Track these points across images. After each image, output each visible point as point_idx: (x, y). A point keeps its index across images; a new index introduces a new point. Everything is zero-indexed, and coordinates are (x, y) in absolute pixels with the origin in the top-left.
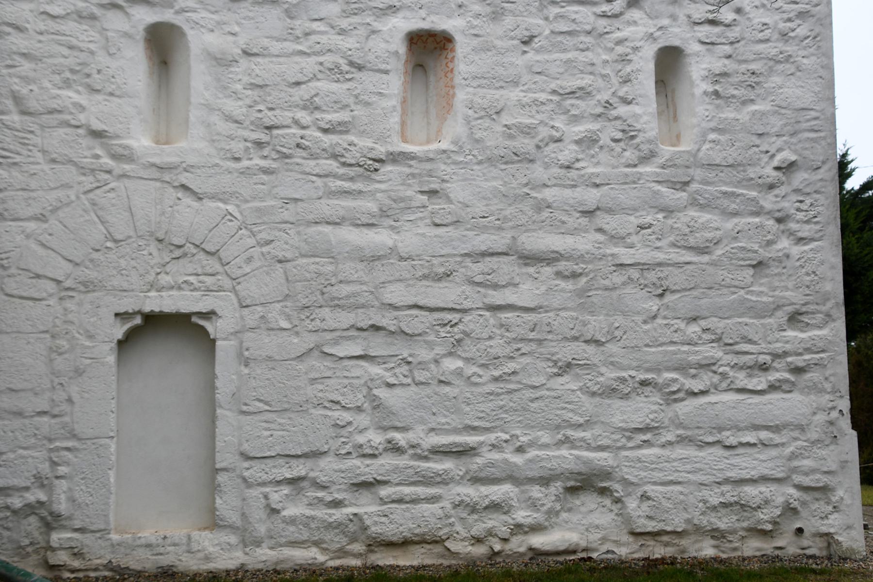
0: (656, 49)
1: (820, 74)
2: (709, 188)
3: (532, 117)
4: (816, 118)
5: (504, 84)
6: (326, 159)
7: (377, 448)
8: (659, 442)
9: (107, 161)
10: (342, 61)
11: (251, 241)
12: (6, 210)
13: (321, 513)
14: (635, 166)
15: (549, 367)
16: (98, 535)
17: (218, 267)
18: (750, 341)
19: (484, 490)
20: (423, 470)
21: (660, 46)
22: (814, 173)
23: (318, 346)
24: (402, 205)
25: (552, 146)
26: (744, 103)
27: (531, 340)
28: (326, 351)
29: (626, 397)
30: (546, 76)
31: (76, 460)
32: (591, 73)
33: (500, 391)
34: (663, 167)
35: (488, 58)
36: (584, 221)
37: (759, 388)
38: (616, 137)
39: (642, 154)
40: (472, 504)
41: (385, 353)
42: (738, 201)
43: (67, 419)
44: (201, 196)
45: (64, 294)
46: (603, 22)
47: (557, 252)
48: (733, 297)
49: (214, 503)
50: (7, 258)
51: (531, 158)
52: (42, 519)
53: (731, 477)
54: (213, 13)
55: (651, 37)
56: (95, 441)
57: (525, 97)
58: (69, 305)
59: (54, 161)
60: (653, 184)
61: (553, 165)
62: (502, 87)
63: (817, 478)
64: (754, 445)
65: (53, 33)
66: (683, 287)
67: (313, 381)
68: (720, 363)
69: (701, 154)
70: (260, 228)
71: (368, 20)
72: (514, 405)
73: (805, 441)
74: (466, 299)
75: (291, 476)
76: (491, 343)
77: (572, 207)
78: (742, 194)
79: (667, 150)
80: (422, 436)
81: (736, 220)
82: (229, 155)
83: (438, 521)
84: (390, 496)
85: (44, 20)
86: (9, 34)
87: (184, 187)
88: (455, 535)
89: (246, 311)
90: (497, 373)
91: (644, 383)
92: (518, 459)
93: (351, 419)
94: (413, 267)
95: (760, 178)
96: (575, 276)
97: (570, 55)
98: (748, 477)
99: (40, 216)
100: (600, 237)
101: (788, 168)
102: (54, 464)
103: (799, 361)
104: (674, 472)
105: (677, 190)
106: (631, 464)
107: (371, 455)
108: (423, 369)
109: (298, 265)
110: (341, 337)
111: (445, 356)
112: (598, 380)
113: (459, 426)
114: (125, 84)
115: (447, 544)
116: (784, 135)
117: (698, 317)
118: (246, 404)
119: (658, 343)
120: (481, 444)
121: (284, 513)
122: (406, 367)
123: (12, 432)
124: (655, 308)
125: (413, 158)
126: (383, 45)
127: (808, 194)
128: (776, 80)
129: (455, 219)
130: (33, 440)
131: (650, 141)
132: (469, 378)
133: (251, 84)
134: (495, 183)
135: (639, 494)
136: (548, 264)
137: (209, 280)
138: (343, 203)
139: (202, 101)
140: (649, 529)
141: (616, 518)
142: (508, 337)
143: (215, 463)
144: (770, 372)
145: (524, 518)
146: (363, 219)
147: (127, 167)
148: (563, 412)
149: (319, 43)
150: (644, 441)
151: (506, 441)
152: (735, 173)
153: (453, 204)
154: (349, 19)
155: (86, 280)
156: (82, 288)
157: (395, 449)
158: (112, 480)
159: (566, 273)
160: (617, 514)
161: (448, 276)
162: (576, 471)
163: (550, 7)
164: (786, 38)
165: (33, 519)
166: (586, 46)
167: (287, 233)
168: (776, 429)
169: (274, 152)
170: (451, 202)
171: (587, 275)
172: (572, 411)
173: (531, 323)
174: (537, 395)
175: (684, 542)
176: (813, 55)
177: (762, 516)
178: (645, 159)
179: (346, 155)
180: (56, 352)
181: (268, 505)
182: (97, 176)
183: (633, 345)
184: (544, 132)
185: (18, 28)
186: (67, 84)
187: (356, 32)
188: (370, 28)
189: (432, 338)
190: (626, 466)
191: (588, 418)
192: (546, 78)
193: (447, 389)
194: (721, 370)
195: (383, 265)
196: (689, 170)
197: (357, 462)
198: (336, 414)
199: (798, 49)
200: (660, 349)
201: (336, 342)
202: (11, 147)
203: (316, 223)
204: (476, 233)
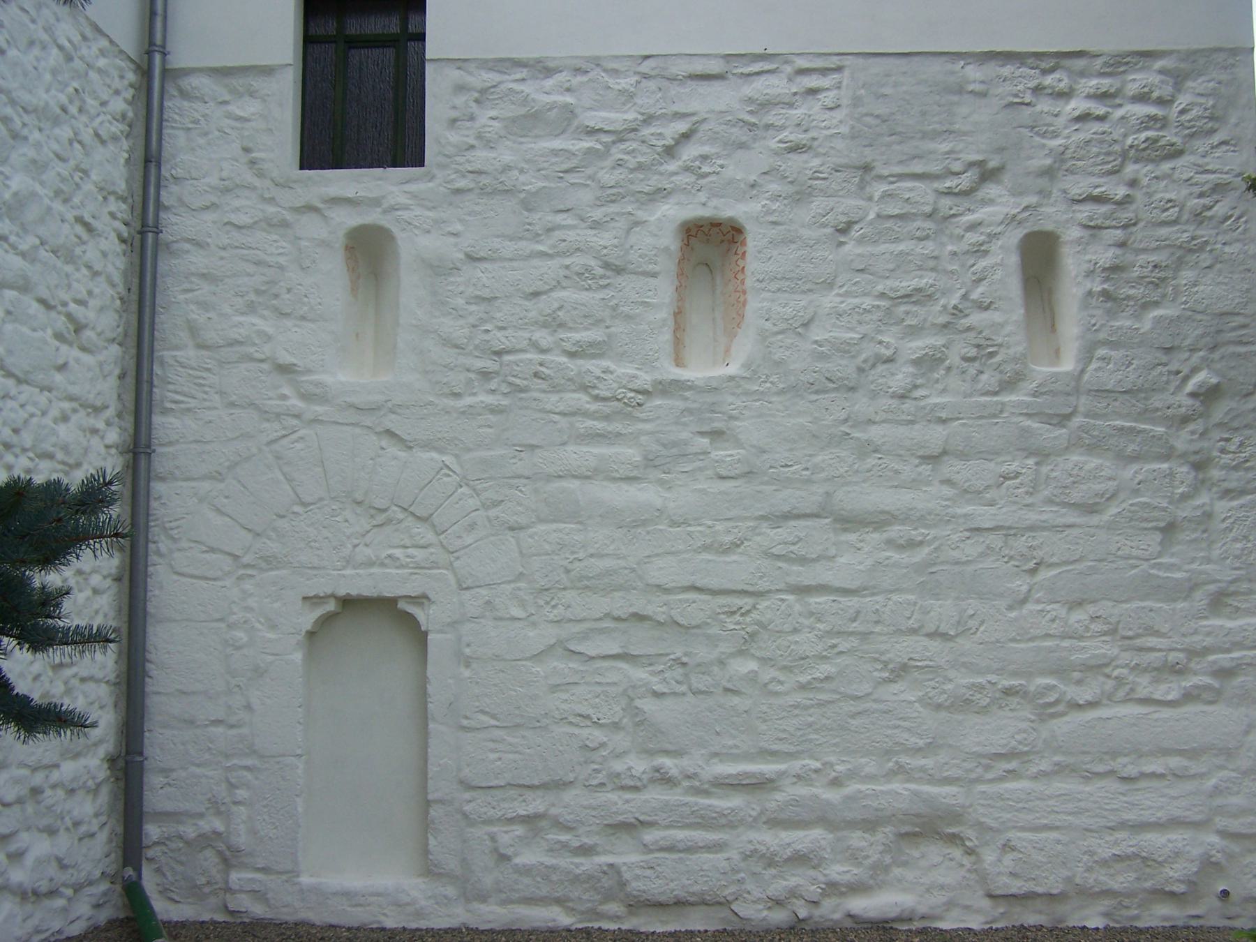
0: (1021, 235)
1: (1248, 267)
2: (1098, 422)
3: (852, 329)
4: (1244, 326)
5: (814, 287)
6: (574, 391)
7: (639, 779)
8: (1029, 772)
9: (296, 403)
10: (593, 263)
11: (473, 502)
12: (177, 467)
13: (565, 862)
14: (996, 393)
15: (876, 670)
16: (284, 877)
17: (430, 537)
18: (1157, 634)
19: (786, 836)
20: (702, 809)
21: (1025, 231)
22: (1243, 401)
23: (561, 642)
24: (674, 451)
25: (881, 368)
26: (1146, 306)
27: (852, 634)
28: (573, 649)
29: (984, 710)
30: (871, 274)
31: (257, 782)
32: (933, 270)
33: (809, 702)
34: (1035, 394)
35: (791, 253)
36: (926, 469)
37: (1170, 697)
38: (969, 355)
39: (1006, 377)
40: (768, 855)
41: (652, 651)
42: (1138, 439)
43: (245, 731)
44: (411, 444)
45: (241, 572)
46: (946, 202)
47: (888, 513)
48: (1133, 572)
49: (427, 845)
50: (177, 527)
51: (851, 385)
52: (220, 853)
53: (1129, 820)
54: (429, 209)
55: (1012, 220)
56: (278, 759)
57: (842, 302)
58: (248, 587)
59: (233, 405)
60: (1021, 419)
61: (882, 393)
62: (810, 290)
63: (1249, 821)
64: (1162, 776)
65: (237, 247)
66: (1064, 559)
67: (555, 688)
68: (1114, 664)
69: (1086, 377)
70: (484, 485)
71: (629, 209)
72: (828, 722)
73: (1233, 770)
74: (761, 578)
75: (525, 813)
76: (796, 638)
77: (909, 450)
78: (1144, 431)
79: (1043, 370)
80: (700, 763)
81: (1135, 467)
82: (446, 390)
83: (721, 877)
84: (657, 841)
85: (228, 232)
86: (188, 252)
87: (390, 433)
88: (745, 895)
89: (467, 595)
90: (804, 679)
91: (1008, 692)
92: (832, 795)
93: (605, 739)
94: (689, 534)
95: (1169, 408)
96: (912, 545)
97: (901, 247)
98: (1153, 819)
99: (214, 474)
100: (947, 491)
101: (1209, 395)
102: (232, 786)
103: (1223, 659)
104: (1049, 812)
105: (1054, 425)
106: (989, 802)
107: (631, 787)
108: (703, 673)
109: (536, 533)
110: (592, 630)
111: (733, 655)
112: (945, 687)
113: (752, 751)
114: (320, 304)
115: (734, 907)
116: (1201, 350)
117: (1084, 600)
118: (467, 718)
119: (1029, 636)
120: (782, 774)
121: (517, 860)
122: (681, 670)
123: (183, 744)
124: (1024, 588)
125: (690, 388)
126: (649, 240)
127: (1237, 429)
128: (1187, 275)
129: (747, 470)
130: (207, 756)
131: (1015, 360)
132: (765, 685)
133: (477, 297)
134: (801, 420)
135: (999, 844)
136: (875, 530)
137: (419, 554)
138: (596, 451)
139: (414, 322)
140: (1014, 891)
141: (968, 875)
142: (820, 630)
143: (427, 793)
145: (839, 874)
146: (621, 471)
147: (319, 409)
148: (896, 731)
149: (564, 241)
150: (1009, 772)
151: (816, 771)
152: (1134, 402)
153: (744, 448)
154: (604, 209)
155: (268, 554)
156: (263, 565)
157: (663, 779)
158: (300, 809)
159: (902, 541)
160: (969, 871)
161: (738, 546)
162: (913, 812)
163: (875, 184)
164: (1199, 218)
165: (209, 853)
166: (925, 234)
167: (521, 491)
168: (1193, 754)
169: (504, 385)
170: (741, 446)
171: (929, 543)
172: (909, 730)
173: (851, 611)
174: (860, 709)
175: (1061, 909)
176: (1238, 240)
177: (1171, 874)
178: (1009, 385)
179: (600, 386)
180: (233, 645)
181: (496, 850)
182: (283, 422)
183: (993, 639)
184: (869, 350)
185: (199, 244)
186: (251, 308)
187: (613, 224)
188: (633, 218)
189: (715, 630)
190: (983, 805)
191: (928, 741)
192: (871, 277)
193: (736, 700)
194: (1116, 673)
195: (648, 533)
196: (1071, 398)
197: (613, 796)
198: (585, 733)
199: (1217, 234)
200: (1031, 644)
201: (585, 636)
202: (185, 389)
203: (560, 477)
204: (774, 488)
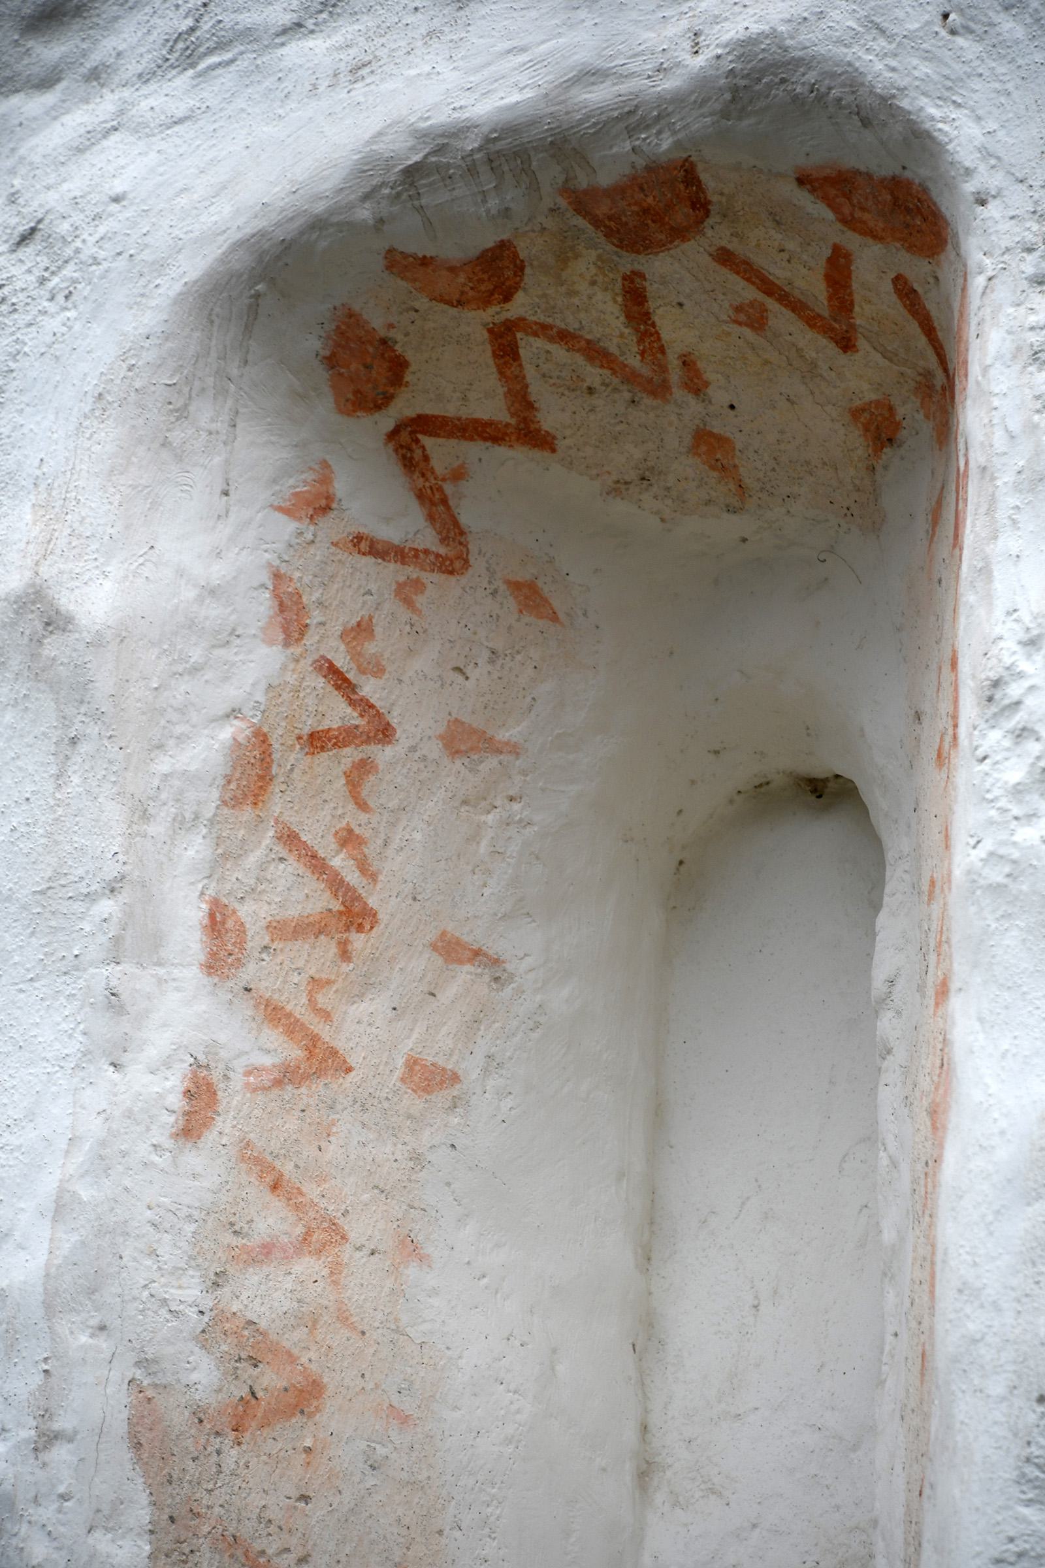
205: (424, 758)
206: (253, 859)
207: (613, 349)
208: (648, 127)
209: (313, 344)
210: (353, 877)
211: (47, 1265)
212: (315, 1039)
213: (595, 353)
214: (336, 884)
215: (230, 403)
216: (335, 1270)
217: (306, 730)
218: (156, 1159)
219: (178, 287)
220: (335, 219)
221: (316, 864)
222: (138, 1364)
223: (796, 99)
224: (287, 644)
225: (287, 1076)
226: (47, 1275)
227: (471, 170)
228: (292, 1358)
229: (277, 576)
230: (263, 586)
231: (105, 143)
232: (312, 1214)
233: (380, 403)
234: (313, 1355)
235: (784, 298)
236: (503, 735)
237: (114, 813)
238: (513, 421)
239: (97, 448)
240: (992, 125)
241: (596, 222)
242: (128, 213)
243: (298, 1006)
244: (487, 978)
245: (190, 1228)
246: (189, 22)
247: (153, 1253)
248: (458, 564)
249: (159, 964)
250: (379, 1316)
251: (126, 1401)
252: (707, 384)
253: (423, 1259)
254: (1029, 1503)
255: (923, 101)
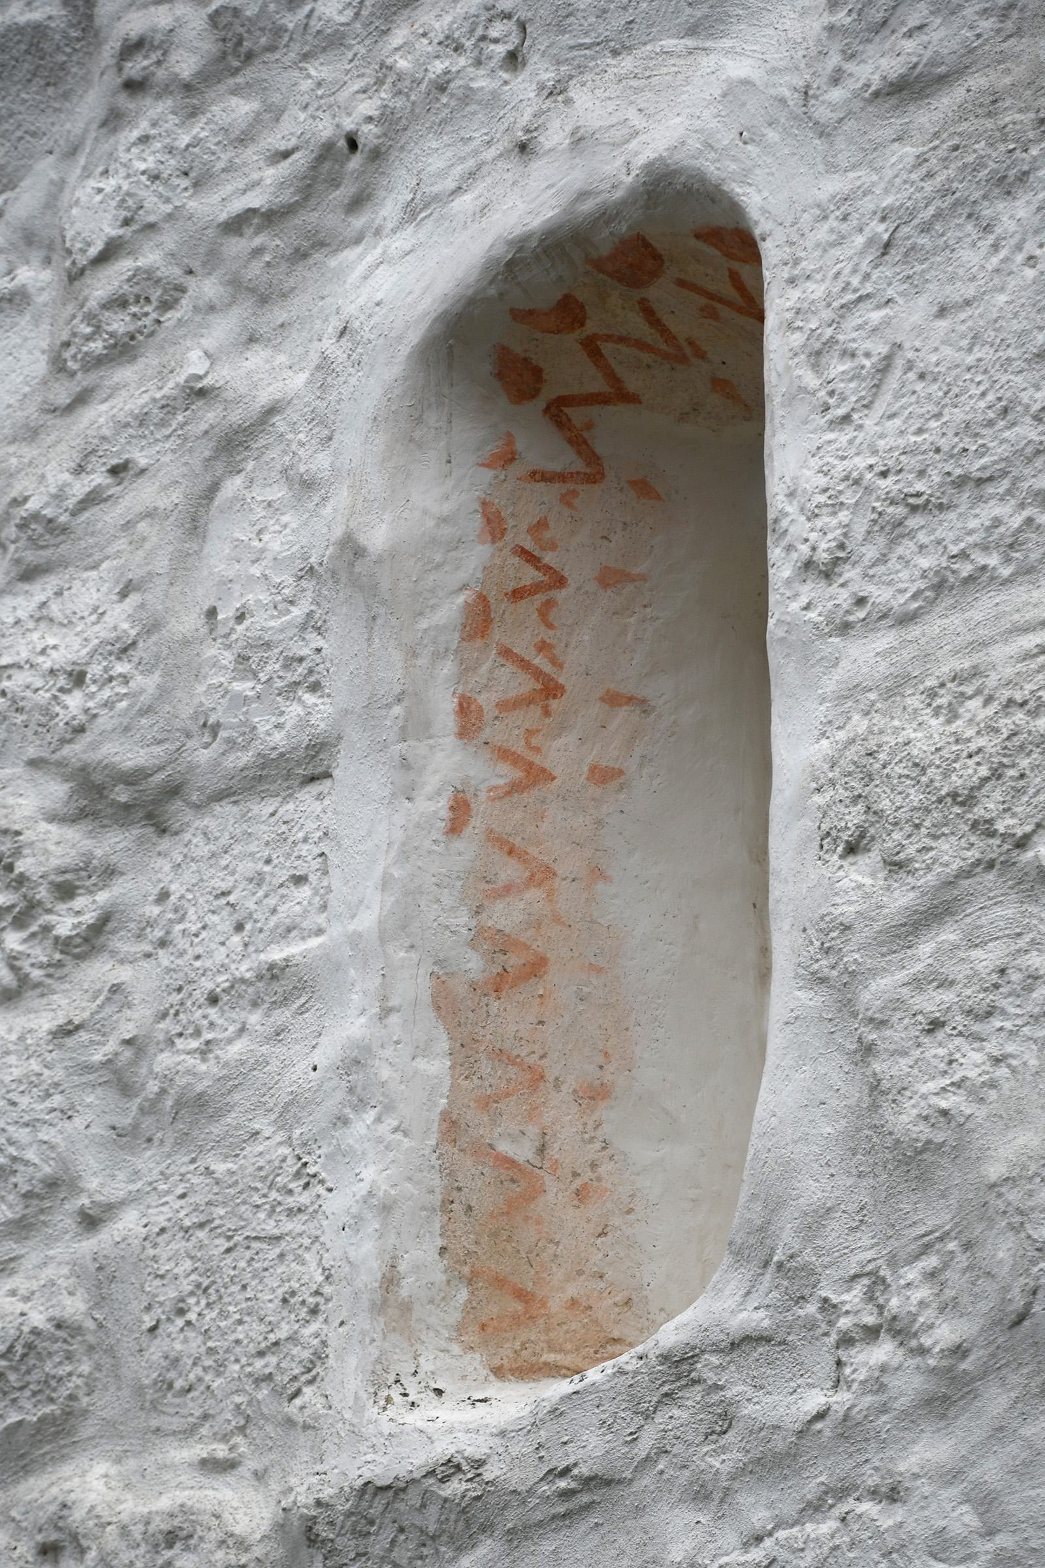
144: (196, 1459)
205: (587, 592)
206: (484, 669)
207: (650, 342)
208: (614, 220)
209: (486, 368)
210: (547, 668)
211: (380, 915)
212: (531, 765)
213: (641, 345)
214: (538, 674)
215: (446, 409)
216: (550, 894)
217: (510, 589)
218: (436, 848)
219: (408, 349)
220: (479, 297)
221: (524, 664)
222: (435, 963)
223: (679, 192)
224: (493, 542)
225: (515, 788)
226: (380, 922)
227: (537, 258)
228: (527, 947)
229: (484, 504)
230: (476, 511)
231: (377, 272)
232: (534, 864)
233: (534, 394)
234: (539, 943)
235: (721, 300)
236: (635, 571)
237: (397, 656)
238: (612, 390)
239: (375, 449)
240: (766, 194)
241: (610, 275)
242: (384, 311)
243: (519, 748)
244: (638, 712)
245: (459, 884)
246: (411, 196)
247: (438, 901)
248: (598, 477)
249: (430, 737)
250: (580, 915)
251: (429, 985)
252: (706, 352)
253: (606, 879)
254: (800, 989)
255: (734, 185)
